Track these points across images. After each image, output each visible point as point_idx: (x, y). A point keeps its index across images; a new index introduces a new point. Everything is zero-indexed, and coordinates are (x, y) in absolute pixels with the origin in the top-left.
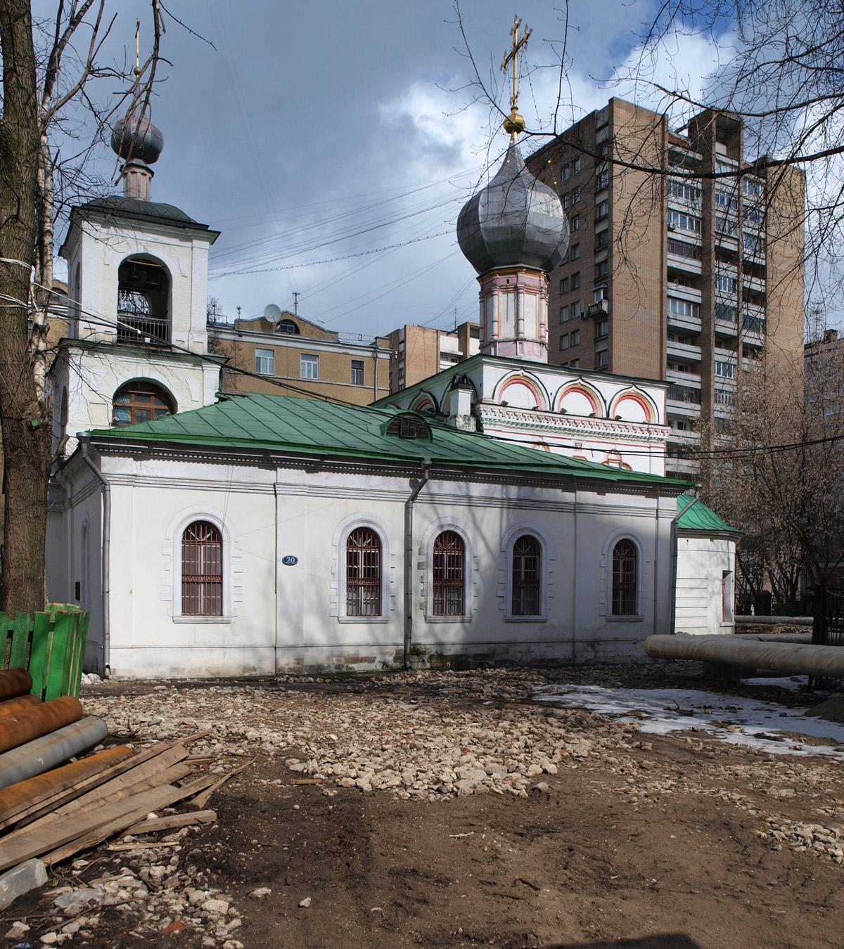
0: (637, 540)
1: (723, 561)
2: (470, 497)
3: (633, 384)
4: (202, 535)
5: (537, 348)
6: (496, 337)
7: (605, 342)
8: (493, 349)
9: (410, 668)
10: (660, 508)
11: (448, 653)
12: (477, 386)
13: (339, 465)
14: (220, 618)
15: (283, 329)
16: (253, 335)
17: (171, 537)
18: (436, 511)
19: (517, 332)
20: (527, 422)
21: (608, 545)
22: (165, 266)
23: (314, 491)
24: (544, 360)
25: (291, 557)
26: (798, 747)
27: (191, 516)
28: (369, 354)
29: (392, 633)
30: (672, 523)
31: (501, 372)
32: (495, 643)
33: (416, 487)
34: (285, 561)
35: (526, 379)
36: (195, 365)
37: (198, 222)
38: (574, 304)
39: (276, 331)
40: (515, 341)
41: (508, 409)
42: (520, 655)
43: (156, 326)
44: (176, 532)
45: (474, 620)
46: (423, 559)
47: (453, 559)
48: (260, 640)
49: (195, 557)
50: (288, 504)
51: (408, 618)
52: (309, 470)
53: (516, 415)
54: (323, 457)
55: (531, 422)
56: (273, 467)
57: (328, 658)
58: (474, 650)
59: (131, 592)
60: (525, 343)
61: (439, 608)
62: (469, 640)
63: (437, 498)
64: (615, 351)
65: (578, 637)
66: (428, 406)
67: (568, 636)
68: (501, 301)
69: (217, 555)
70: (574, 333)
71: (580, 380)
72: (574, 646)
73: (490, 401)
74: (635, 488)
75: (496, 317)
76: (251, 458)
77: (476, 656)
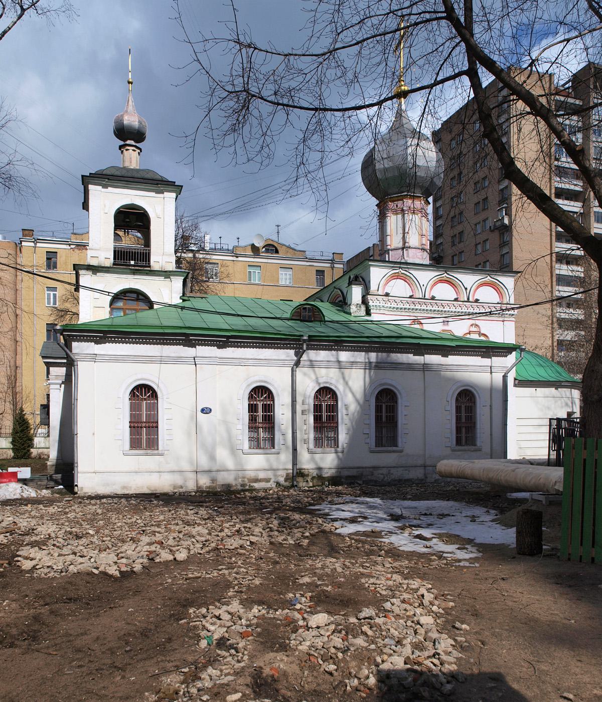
0: (475, 389)
1: (567, 405)
2: (339, 362)
3: (488, 274)
4: (143, 393)
5: (419, 253)
6: (389, 247)
7: (507, 247)
8: (387, 256)
9: (296, 486)
10: (493, 365)
11: (326, 476)
12: (367, 282)
13: (241, 342)
14: (156, 452)
15: (267, 251)
16: (245, 256)
17: (121, 396)
18: (314, 372)
19: (404, 242)
20: (405, 307)
21: (451, 395)
22: (146, 212)
23: (223, 362)
24: (427, 262)
25: (207, 408)
26: (428, 546)
27: (135, 381)
28: (329, 265)
29: (282, 461)
30: (504, 376)
31: (384, 271)
32: (363, 468)
33: (299, 355)
34: (203, 411)
35: (404, 276)
36: (165, 278)
37: (170, 180)
38: (484, 221)
39: (262, 252)
40: (403, 249)
41: (390, 298)
42: (382, 476)
43: (141, 253)
44: (125, 392)
45: (345, 451)
46: (306, 407)
47: (468, 408)
48: (186, 466)
49: (140, 409)
50: (205, 370)
51: (295, 450)
52: (219, 347)
53: (396, 302)
54: (228, 337)
55: (408, 306)
56: (194, 346)
57: (236, 479)
58: (346, 473)
59: (94, 434)
60: (410, 250)
61: (318, 442)
62: (342, 466)
63: (315, 363)
64: (514, 254)
65: (428, 463)
66: (338, 300)
67: (420, 462)
68: (393, 221)
69: (154, 408)
70: (485, 241)
71: (445, 274)
72: (425, 469)
73: (376, 293)
74: (471, 351)
75: (388, 232)
76: (176, 340)
77: (348, 477)
